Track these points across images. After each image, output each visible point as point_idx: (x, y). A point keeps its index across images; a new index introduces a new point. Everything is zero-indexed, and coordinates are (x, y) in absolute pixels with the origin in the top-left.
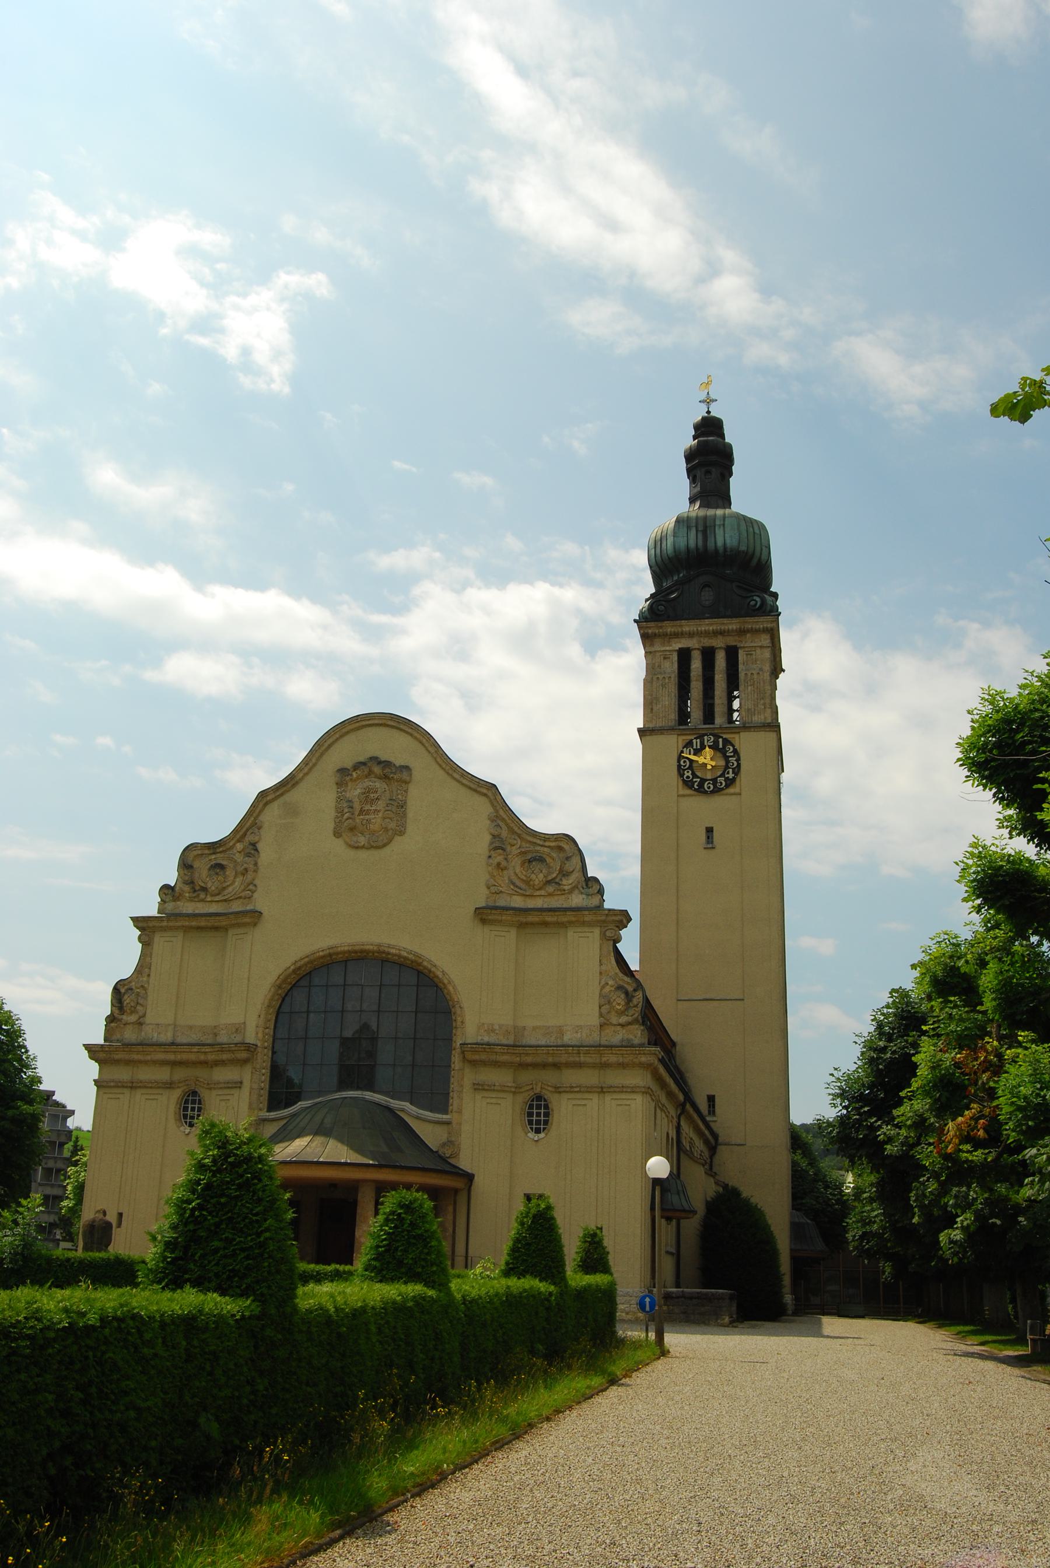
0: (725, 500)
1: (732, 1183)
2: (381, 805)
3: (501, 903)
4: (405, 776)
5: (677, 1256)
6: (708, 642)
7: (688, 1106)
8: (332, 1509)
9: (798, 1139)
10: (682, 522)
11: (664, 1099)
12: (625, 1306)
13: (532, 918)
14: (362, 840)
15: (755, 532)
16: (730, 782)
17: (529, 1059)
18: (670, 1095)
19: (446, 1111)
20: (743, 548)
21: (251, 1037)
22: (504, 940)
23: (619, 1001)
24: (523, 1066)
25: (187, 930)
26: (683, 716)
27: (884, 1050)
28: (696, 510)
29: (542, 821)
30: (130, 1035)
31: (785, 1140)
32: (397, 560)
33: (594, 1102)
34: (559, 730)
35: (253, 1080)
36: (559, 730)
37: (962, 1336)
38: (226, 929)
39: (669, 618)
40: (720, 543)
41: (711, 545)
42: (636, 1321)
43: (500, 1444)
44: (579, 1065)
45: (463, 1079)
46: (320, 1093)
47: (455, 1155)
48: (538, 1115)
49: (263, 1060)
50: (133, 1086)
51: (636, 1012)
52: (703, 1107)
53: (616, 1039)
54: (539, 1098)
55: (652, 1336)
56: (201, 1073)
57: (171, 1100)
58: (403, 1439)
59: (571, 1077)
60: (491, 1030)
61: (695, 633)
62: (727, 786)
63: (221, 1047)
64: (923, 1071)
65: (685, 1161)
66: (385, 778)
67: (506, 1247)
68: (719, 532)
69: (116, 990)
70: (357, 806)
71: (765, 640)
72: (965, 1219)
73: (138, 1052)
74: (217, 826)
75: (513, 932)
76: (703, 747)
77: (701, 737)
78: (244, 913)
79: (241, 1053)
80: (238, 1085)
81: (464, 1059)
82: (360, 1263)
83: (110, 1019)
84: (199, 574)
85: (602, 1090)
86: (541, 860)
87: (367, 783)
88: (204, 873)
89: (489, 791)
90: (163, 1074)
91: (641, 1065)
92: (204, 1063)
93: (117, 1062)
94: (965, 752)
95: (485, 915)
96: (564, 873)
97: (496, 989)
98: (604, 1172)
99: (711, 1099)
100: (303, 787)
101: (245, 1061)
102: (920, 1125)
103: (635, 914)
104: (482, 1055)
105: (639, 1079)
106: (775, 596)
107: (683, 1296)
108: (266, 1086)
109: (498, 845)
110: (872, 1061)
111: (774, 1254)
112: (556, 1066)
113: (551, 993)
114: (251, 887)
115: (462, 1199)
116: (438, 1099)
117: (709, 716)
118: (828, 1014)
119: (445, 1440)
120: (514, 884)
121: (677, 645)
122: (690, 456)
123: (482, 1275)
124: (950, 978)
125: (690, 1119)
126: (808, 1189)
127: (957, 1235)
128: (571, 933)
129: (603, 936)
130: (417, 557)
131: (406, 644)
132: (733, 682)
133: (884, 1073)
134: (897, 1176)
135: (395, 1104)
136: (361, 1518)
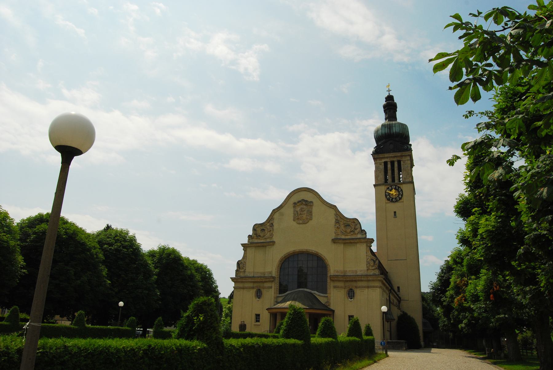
1: (406, 311)
2: (305, 212)
3: (339, 237)
4: (311, 204)
5: (390, 331)
6: (392, 159)
9: (423, 297)
11: (385, 289)
12: (377, 345)
14: (301, 222)
15: (404, 128)
16: (400, 199)
17: (348, 279)
18: (387, 288)
19: (326, 293)
21: (274, 275)
24: (347, 281)
25: (255, 247)
26: (386, 180)
27: (443, 277)
28: (387, 122)
29: (348, 214)
30: (242, 275)
31: (419, 298)
33: (366, 291)
34: (353, 189)
36: (353, 189)
37: (470, 353)
38: (266, 246)
40: (394, 131)
41: (392, 132)
42: (380, 349)
44: (362, 281)
45: (330, 285)
47: (329, 305)
48: (351, 294)
49: (277, 281)
50: (243, 288)
51: (377, 266)
52: (396, 289)
53: (372, 273)
54: (351, 289)
55: (384, 352)
56: (261, 285)
57: (253, 292)
60: (338, 272)
61: (388, 157)
64: (452, 284)
66: (306, 205)
67: (347, 330)
69: (238, 263)
70: (299, 213)
71: (408, 158)
72: (465, 321)
74: (262, 220)
75: (342, 245)
77: (391, 186)
78: (270, 242)
79: (271, 279)
80: (271, 287)
82: (317, 333)
83: (237, 271)
85: (368, 287)
86: (349, 225)
87: (301, 206)
88: (259, 232)
89: (334, 207)
90: (251, 285)
91: (379, 280)
92: (262, 282)
93: (239, 282)
94: (456, 209)
95: (335, 241)
96: (355, 229)
97: (338, 260)
98: (371, 308)
99: (398, 288)
100: (284, 208)
101: (273, 281)
102: (452, 297)
103: (375, 239)
104: (335, 278)
105: (378, 284)
106: (411, 145)
109: (337, 222)
111: (418, 330)
112: (355, 281)
113: (354, 261)
114: (272, 235)
116: (324, 290)
117: (393, 180)
121: (383, 161)
122: (385, 107)
123: (343, 336)
124: (457, 259)
125: (393, 294)
126: (427, 312)
127: (463, 325)
128: (358, 245)
129: (367, 246)
134: (448, 310)
135: (313, 292)
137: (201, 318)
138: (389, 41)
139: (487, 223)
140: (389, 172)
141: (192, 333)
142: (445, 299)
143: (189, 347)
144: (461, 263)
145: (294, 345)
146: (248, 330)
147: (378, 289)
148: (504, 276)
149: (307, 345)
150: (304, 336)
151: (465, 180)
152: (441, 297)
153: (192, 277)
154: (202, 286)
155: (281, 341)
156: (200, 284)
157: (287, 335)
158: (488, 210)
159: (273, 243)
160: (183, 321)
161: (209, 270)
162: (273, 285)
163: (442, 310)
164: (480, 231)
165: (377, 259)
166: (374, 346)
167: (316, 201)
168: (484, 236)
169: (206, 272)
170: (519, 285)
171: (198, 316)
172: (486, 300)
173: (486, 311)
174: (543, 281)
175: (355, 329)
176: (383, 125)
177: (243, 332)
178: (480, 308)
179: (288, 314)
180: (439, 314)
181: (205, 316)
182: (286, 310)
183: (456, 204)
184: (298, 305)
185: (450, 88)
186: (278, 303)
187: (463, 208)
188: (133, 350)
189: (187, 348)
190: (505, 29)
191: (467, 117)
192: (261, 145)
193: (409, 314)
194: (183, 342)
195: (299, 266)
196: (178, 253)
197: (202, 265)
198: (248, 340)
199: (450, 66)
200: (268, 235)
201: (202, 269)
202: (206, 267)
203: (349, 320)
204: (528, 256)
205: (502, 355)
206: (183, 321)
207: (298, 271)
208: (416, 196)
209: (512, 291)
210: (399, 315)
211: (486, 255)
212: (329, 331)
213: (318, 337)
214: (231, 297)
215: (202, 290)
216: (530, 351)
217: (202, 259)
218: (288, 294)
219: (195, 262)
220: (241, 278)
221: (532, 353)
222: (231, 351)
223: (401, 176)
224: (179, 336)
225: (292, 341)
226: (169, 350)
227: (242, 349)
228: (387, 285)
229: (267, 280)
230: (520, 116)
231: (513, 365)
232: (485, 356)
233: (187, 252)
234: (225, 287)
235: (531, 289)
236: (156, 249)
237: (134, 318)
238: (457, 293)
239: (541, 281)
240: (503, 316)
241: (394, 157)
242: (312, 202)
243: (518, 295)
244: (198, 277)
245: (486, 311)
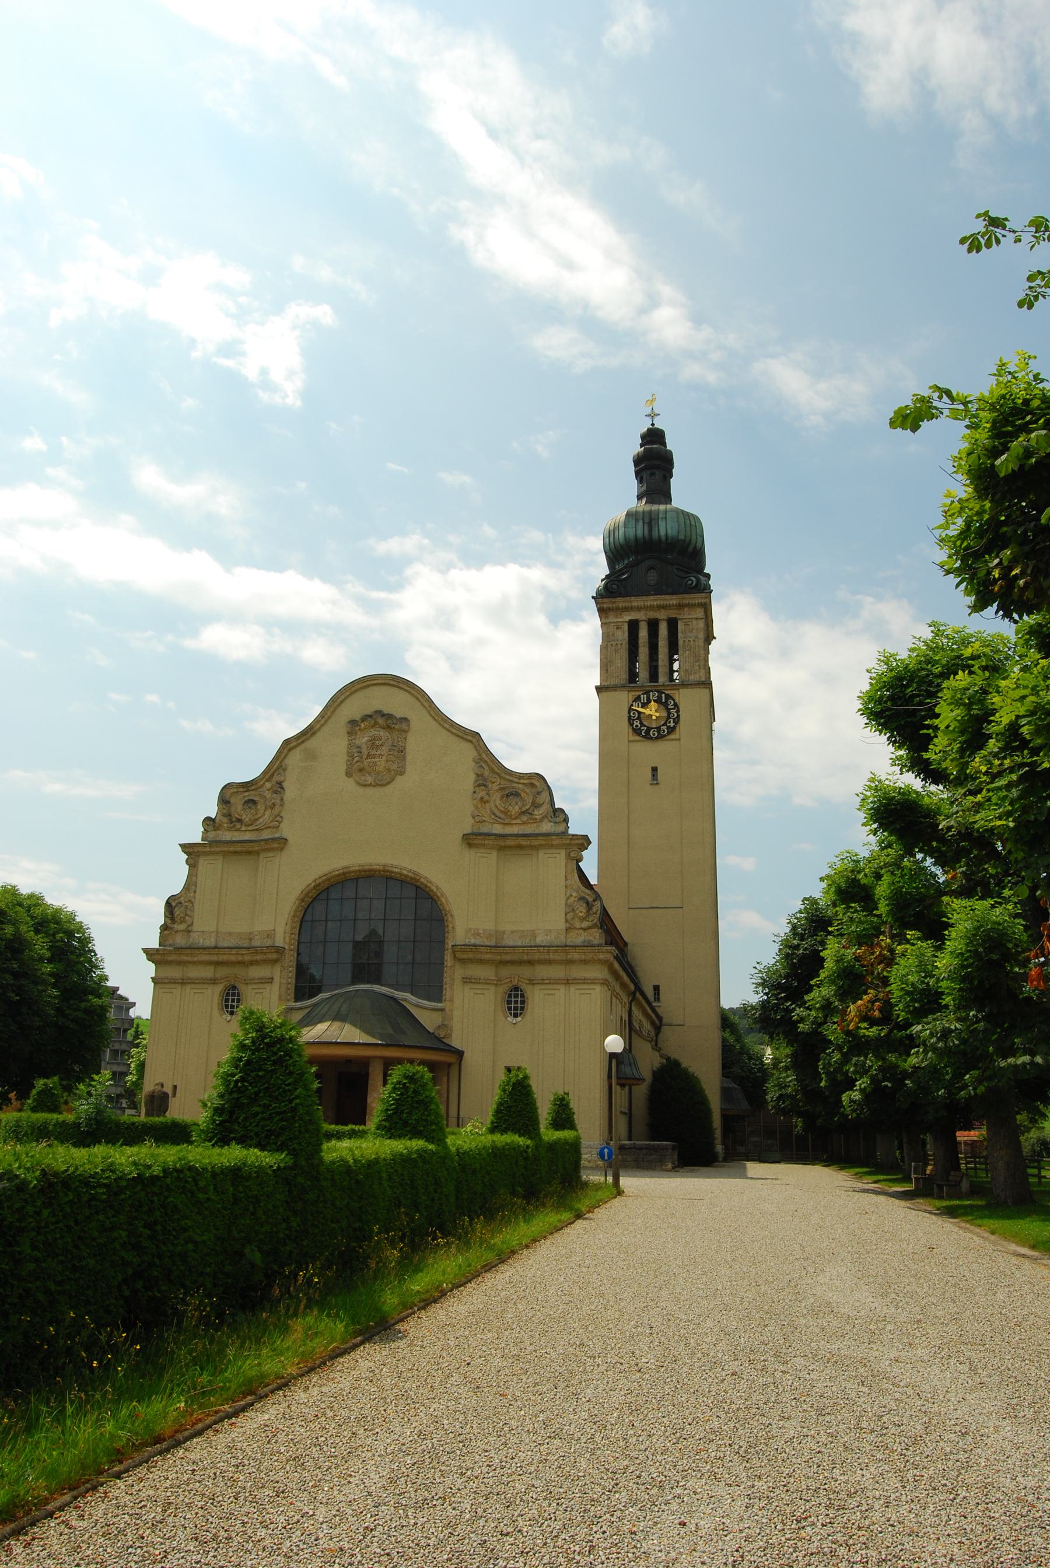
0: (667, 498)
1: (674, 1056)
2: (384, 750)
3: (485, 829)
4: (404, 726)
5: (629, 1115)
6: (653, 615)
7: (638, 994)
8: (354, 1320)
9: (726, 1020)
11: (618, 989)
12: (588, 1155)
14: (370, 779)
15: (691, 523)
16: (671, 730)
17: (508, 958)
18: (623, 985)
19: (440, 1001)
20: (682, 537)
21: (279, 942)
23: (582, 909)
25: (226, 854)
26: (633, 676)
28: (643, 506)
29: (517, 762)
30: (180, 940)
31: (716, 1021)
34: (532, 690)
35: (282, 976)
36: (532, 690)
37: (859, 1176)
39: (621, 595)
40: (662, 533)
41: (655, 534)
42: (596, 1168)
43: (489, 1267)
44: (549, 962)
45: (454, 973)
47: (449, 1036)
49: (290, 959)
50: (183, 982)
51: (595, 919)
54: (516, 989)
55: (610, 1179)
56: (239, 971)
57: (215, 993)
58: (410, 1264)
61: (643, 607)
62: (669, 733)
63: (256, 950)
64: (829, 964)
65: (636, 1039)
66: (388, 727)
68: (662, 524)
69: (168, 904)
70: (365, 751)
71: (700, 613)
73: (187, 955)
74: (250, 770)
75: (494, 854)
76: (649, 701)
77: (647, 693)
78: (273, 840)
79: (273, 954)
80: (270, 981)
83: (164, 928)
85: (567, 982)
86: (517, 794)
87: (373, 732)
88: (240, 807)
89: (473, 738)
90: (208, 972)
94: (865, 703)
95: (471, 840)
96: (536, 805)
97: (482, 898)
98: (571, 1047)
99: (656, 988)
100: (319, 735)
102: (827, 1008)
105: (599, 972)
106: (708, 576)
107: (634, 1147)
109: (481, 782)
110: (787, 956)
111: (708, 1112)
112: (530, 963)
113: (526, 904)
114: (278, 819)
115: (456, 1067)
116: (434, 990)
117: (654, 676)
119: (445, 1264)
120: (494, 814)
121: (627, 618)
122: (638, 461)
123: (472, 1133)
125: (639, 1004)
126: (735, 1060)
127: (856, 1095)
129: (568, 856)
133: (798, 967)
135: (398, 994)
136: (377, 1328)
140: (643, 652)
145: (236, 1173)
147: (598, 988)
149: (305, 1173)
151: (946, 527)
154: (51, 974)
156: (48, 968)
159: (283, 842)
161: (80, 928)
162: (276, 972)
165: (598, 897)
167: (418, 719)
169: (70, 934)
175: (516, 1105)
177: (157, 1119)
178: (946, 1033)
184: (349, 1033)
191: (973, 244)
193: (684, 1066)
197: (58, 911)
200: (266, 817)
201: (58, 923)
202: (72, 917)
208: (715, 725)
211: (1025, 810)
215: (54, 986)
216: (1035, 1171)
219: (35, 901)
220: (175, 952)
223: (676, 666)
225: (233, 1154)
229: (258, 958)
240: (1026, 1059)
241: (660, 607)
242: (406, 719)
244: (40, 945)
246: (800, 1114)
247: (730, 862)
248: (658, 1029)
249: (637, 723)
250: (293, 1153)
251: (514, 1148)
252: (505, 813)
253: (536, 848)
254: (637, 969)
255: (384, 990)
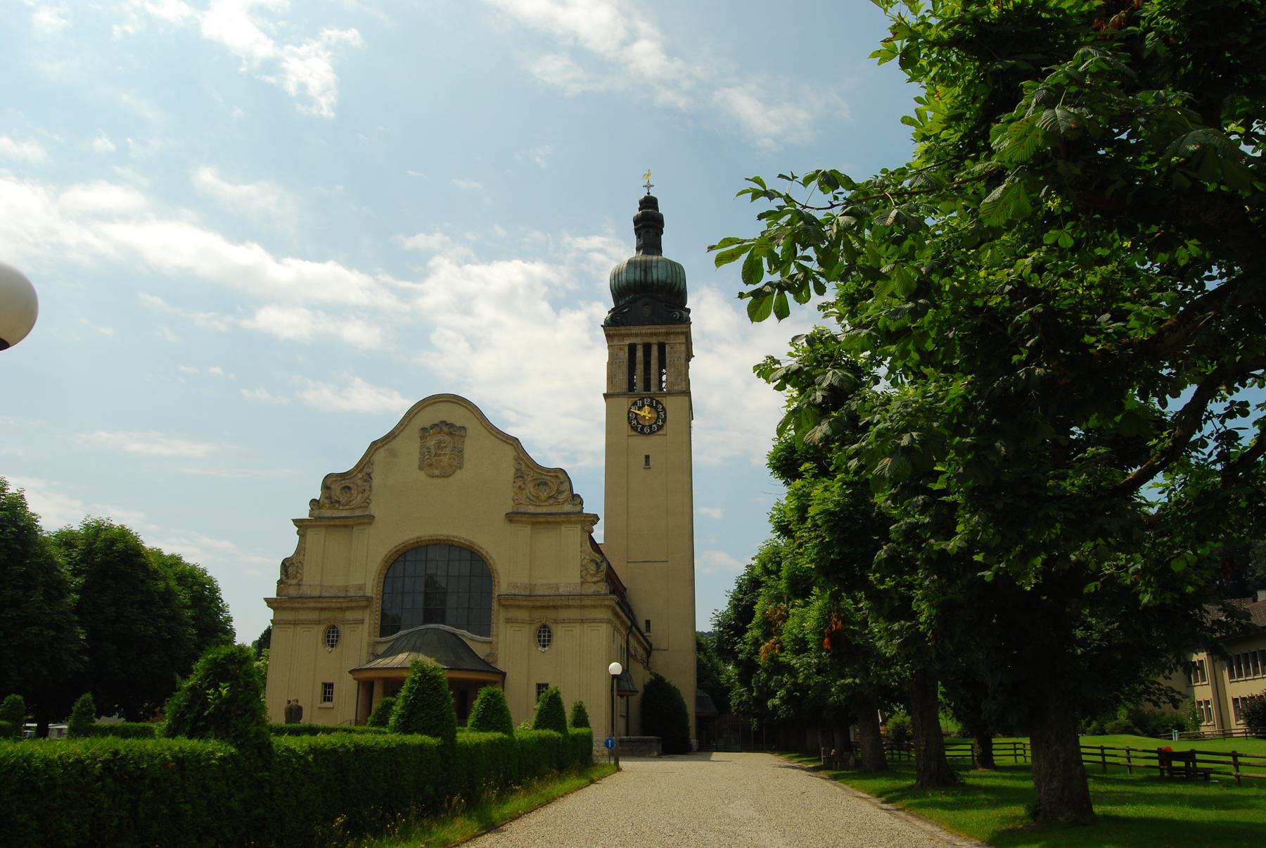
0: (658, 250)
1: (661, 674)
2: (447, 451)
3: (522, 509)
4: (462, 433)
5: (627, 717)
6: (647, 340)
8: (481, 822)
9: (700, 643)
10: (631, 263)
12: (598, 748)
13: (541, 519)
14: (437, 472)
15: (676, 271)
16: (660, 428)
17: (539, 604)
18: (623, 622)
21: (369, 592)
22: (523, 532)
23: (593, 568)
25: (327, 527)
26: (631, 386)
27: (741, 600)
28: (640, 256)
30: (292, 592)
31: (690, 646)
32: (419, 241)
33: (577, 628)
34: (547, 385)
35: (371, 618)
36: (547, 385)
37: (790, 759)
38: (352, 526)
39: (623, 325)
41: (649, 278)
42: (603, 755)
43: (542, 805)
44: (568, 607)
45: (499, 615)
46: (412, 626)
49: (377, 606)
50: (295, 623)
51: (602, 575)
52: (643, 627)
58: (501, 799)
59: (564, 614)
61: (639, 334)
63: (351, 599)
65: (632, 663)
66: (450, 434)
68: (654, 271)
69: (283, 564)
70: (433, 451)
71: (682, 339)
74: (346, 464)
76: (643, 405)
77: (642, 399)
78: (363, 516)
79: (363, 602)
80: (362, 621)
81: (500, 604)
82: (470, 722)
83: (280, 583)
84: (279, 248)
85: (582, 621)
86: (545, 484)
87: (440, 437)
88: (338, 491)
89: (514, 442)
90: (314, 616)
91: (606, 606)
93: (285, 609)
95: (511, 517)
96: (560, 492)
97: (520, 561)
98: (586, 667)
99: (648, 622)
101: (366, 607)
102: (756, 643)
104: (510, 601)
105: (605, 614)
106: (689, 311)
107: (630, 741)
108: (379, 622)
109: (519, 475)
110: (735, 607)
111: (685, 715)
112: (555, 607)
113: (554, 564)
114: (366, 503)
116: (484, 627)
117: (647, 386)
118: (721, 558)
119: (517, 802)
121: (628, 341)
123: (524, 728)
124: (770, 563)
125: (634, 635)
126: (705, 675)
127: (777, 701)
128: (563, 528)
129: (583, 530)
130: (435, 240)
131: (427, 302)
132: (662, 364)
133: (741, 612)
134: (748, 669)
135: (458, 631)
136: (491, 827)
137: (224, 692)
138: (647, 55)
139: (827, 495)
141: (202, 724)
142: (743, 648)
143: (199, 755)
144: (777, 572)
145: (421, 748)
146: (305, 721)
147: (604, 625)
148: (857, 602)
150: (444, 729)
152: (735, 643)
153: (168, 596)
154: (192, 618)
155: (389, 738)
156: (189, 613)
157: (405, 727)
158: (831, 469)
160: (179, 699)
161: (211, 580)
162: (366, 615)
163: (736, 671)
164: (812, 511)
165: (604, 559)
166: (590, 750)
168: (819, 522)
169: (203, 585)
170: (881, 619)
171: (216, 687)
172: (820, 649)
173: (819, 672)
174: (925, 611)
175: (551, 711)
176: (630, 263)
179: (407, 681)
180: (730, 678)
181: (231, 686)
182: (405, 674)
183: (772, 449)
185: (741, 295)
186: (378, 657)
187: (786, 459)
188: (79, 761)
189: (197, 756)
190: (833, 206)
192: (333, 277)
194: (184, 744)
195: (429, 572)
196: (136, 538)
197: (194, 568)
198: (321, 739)
199: (744, 257)
201: (194, 577)
202: (204, 572)
203: (539, 694)
204: (893, 565)
205: (851, 761)
206: (179, 699)
207: (427, 586)
208: (693, 422)
209: (871, 631)
210: (647, 681)
211: (821, 559)
212: (496, 716)
213: (471, 731)
214: (265, 640)
215: (193, 626)
217: (193, 555)
218: (401, 636)
219: (175, 561)
221: (909, 756)
222: (288, 760)
223: (664, 378)
224: (172, 733)
225: (416, 739)
226: (156, 761)
227: (310, 758)
228: (624, 617)
229: (353, 604)
230: (864, 332)
231: (868, 779)
232: (818, 764)
233: (160, 536)
234: (248, 620)
235: (902, 626)
236: (76, 527)
237: (19, 697)
238: (767, 635)
239: (921, 613)
240: (850, 680)
241: (652, 334)
242: (464, 428)
243: (880, 638)
244: (184, 596)
245: (819, 672)
246: (755, 716)
247: (705, 512)
248: (649, 653)
249: (634, 422)
250: (444, 738)
251: (552, 738)
252: (537, 497)
253: (560, 523)
254: (634, 609)
255: (447, 628)
